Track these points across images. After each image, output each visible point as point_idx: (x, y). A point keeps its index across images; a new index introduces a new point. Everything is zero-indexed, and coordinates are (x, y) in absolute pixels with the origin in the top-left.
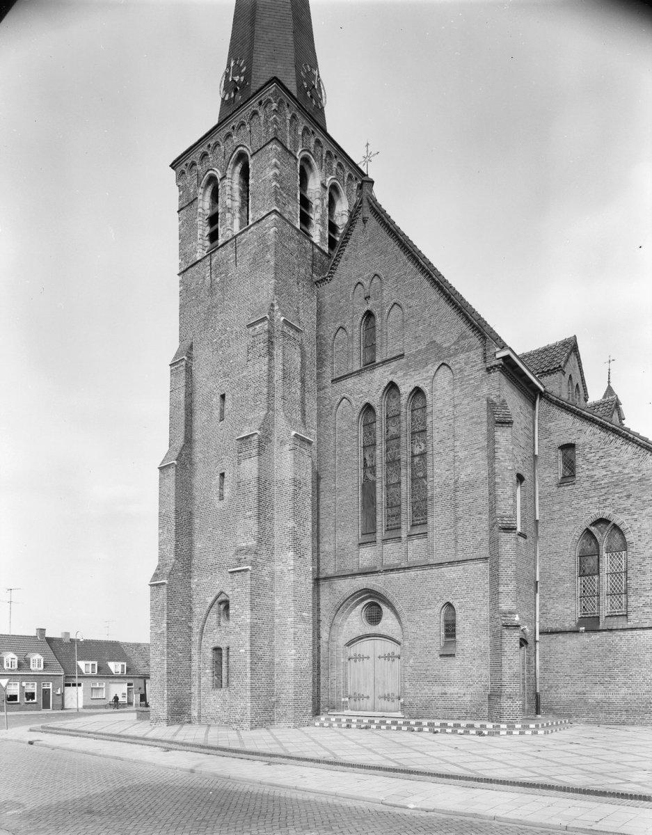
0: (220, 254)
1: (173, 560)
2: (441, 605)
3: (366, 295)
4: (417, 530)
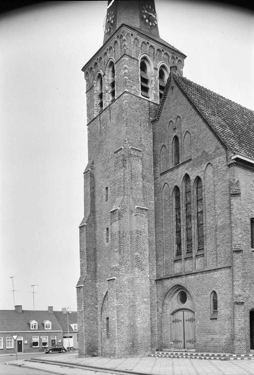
0: (104, 114)
1: (86, 274)
2: (210, 292)
3: (174, 127)
4: (200, 253)
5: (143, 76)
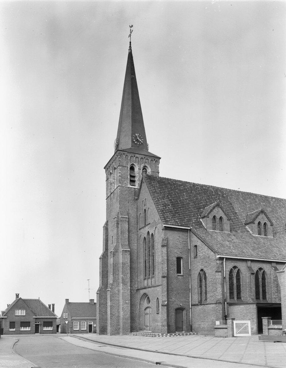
5: (131, 175)
